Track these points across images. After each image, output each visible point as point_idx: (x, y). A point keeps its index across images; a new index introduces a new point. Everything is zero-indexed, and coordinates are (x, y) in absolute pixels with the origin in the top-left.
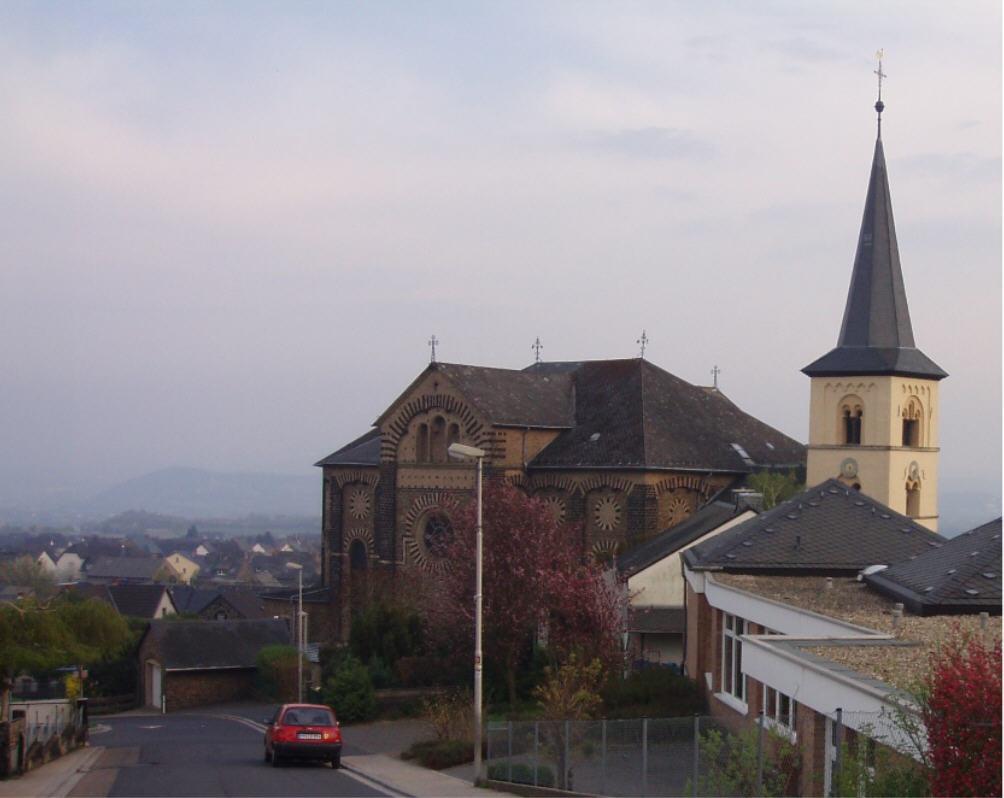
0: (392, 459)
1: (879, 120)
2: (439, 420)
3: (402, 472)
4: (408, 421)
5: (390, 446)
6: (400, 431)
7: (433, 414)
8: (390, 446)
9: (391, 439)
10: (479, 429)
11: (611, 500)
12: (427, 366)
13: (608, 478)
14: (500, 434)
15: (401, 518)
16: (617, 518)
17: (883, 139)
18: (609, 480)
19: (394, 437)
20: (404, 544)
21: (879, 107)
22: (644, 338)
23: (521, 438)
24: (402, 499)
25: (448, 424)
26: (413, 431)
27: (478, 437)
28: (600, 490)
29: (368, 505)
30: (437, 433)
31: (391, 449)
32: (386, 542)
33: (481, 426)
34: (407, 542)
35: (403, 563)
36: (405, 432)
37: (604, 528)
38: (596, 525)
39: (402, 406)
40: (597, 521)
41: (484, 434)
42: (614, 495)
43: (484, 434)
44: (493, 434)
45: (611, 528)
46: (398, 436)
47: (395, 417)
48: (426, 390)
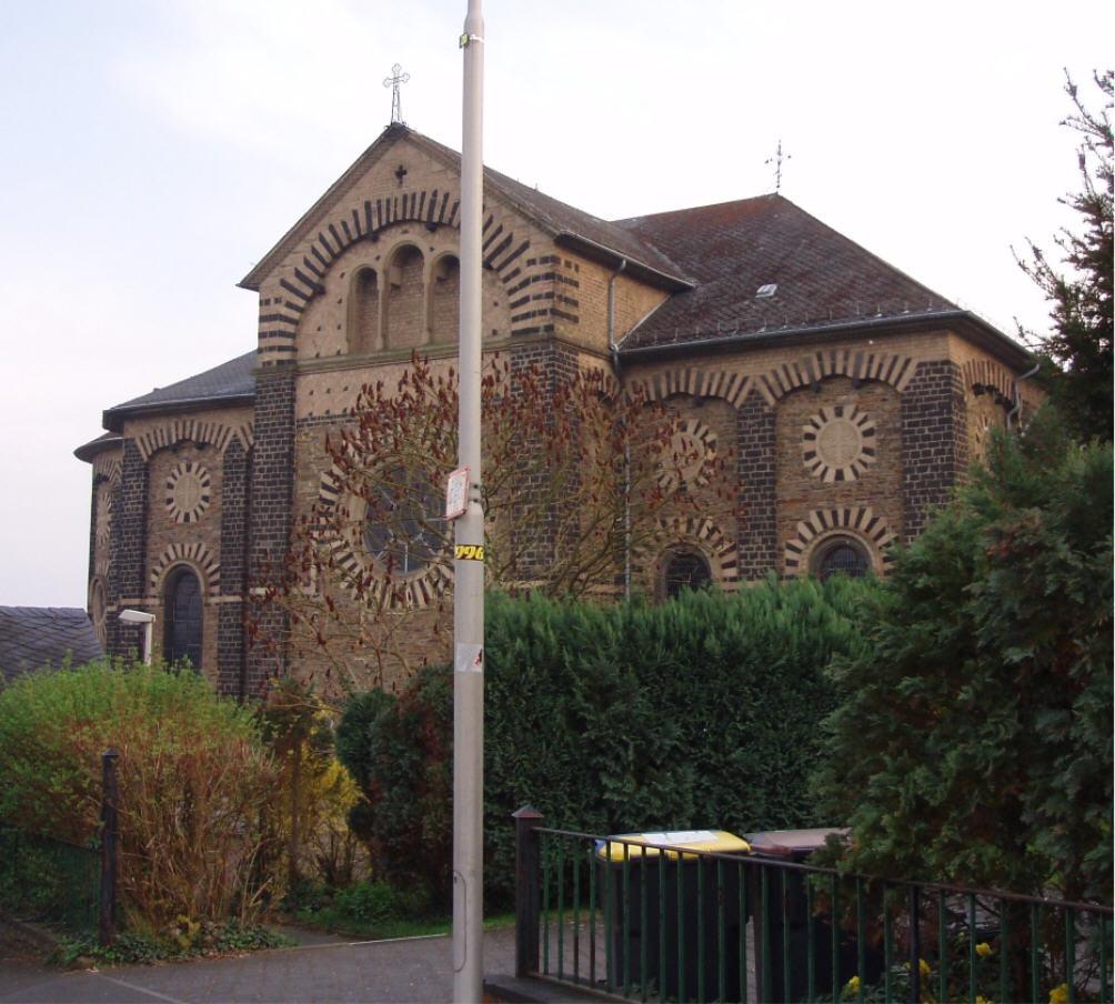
0: (286, 356)
2: (409, 255)
3: (306, 383)
4: (328, 266)
5: (282, 326)
6: (308, 291)
7: (392, 240)
8: (282, 326)
9: (284, 311)
10: (517, 254)
11: (848, 410)
13: (840, 356)
14: (568, 264)
16: (867, 451)
18: (845, 360)
19: (290, 305)
22: (779, 154)
23: (605, 285)
25: (430, 259)
26: (340, 284)
27: (516, 272)
28: (815, 388)
29: (207, 491)
30: (396, 287)
31: (282, 334)
33: (525, 246)
36: (320, 291)
37: (830, 477)
38: (805, 473)
39: (313, 235)
40: (809, 464)
41: (531, 262)
42: (854, 396)
43: (531, 262)
44: (555, 260)
45: (849, 476)
46: (301, 303)
47: (295, 261)
48: (379, 187)
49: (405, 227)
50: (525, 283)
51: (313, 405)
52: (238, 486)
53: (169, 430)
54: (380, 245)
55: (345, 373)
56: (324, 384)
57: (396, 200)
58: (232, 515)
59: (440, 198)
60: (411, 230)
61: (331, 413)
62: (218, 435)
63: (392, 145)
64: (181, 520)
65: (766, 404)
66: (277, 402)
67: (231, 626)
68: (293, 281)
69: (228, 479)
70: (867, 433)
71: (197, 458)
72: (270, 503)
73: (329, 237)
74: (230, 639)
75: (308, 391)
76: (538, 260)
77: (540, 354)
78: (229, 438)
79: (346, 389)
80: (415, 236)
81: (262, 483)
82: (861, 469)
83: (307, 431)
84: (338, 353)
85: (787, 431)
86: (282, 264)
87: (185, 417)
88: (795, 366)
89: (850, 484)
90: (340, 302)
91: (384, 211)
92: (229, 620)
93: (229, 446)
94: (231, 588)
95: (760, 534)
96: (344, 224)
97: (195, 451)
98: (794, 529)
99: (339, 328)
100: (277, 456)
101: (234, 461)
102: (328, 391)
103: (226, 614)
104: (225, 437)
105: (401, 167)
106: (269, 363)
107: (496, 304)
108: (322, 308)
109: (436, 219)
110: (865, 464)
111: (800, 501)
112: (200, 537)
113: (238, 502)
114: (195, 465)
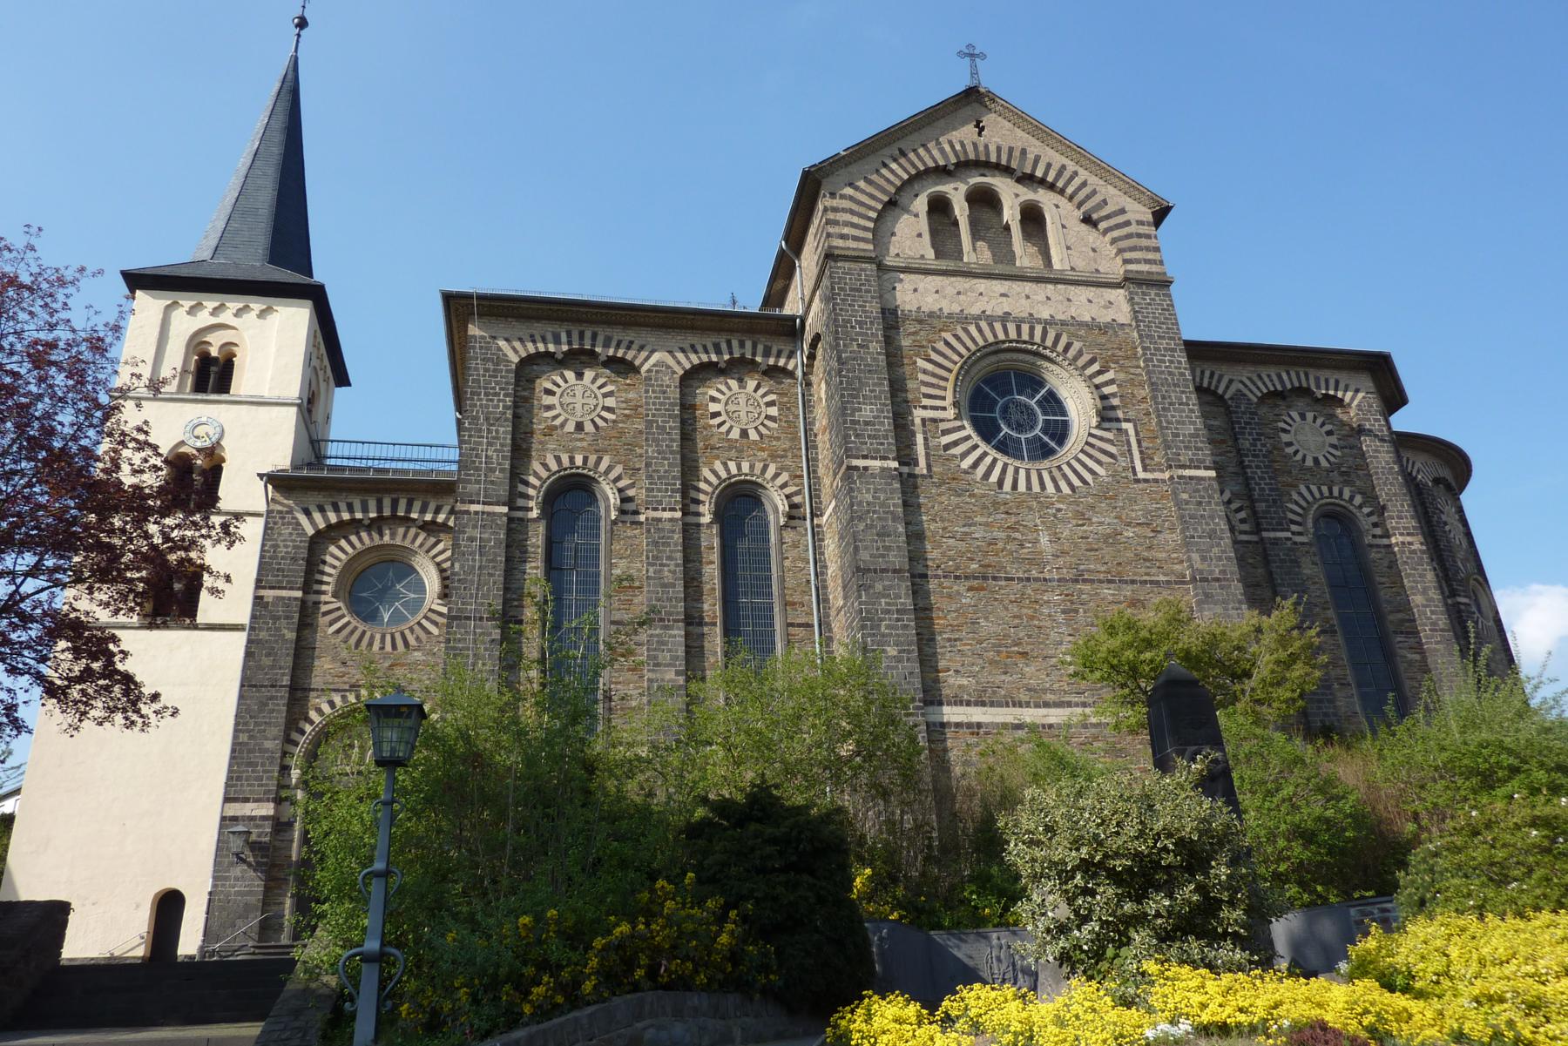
99: (920, 235)
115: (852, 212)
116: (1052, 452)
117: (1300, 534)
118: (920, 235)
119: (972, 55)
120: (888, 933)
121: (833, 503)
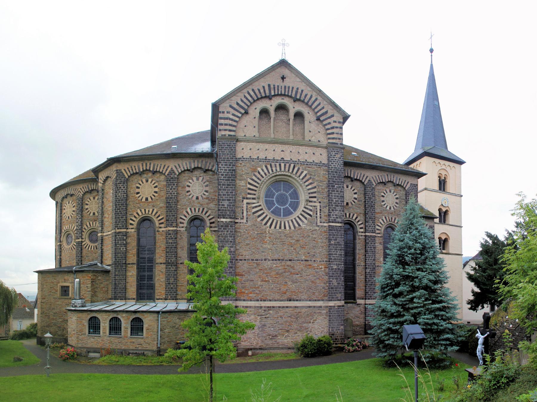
1: (432, 56)
3: (240, 146)
8: (231, 122)
10: (329, 118)
12: (278, 61)
15: (241, 183)
16: (397, 203)
17: (433, 63)
20: (245, 206)
21: (432, 51)
24: (242, 169)
26: (255, 111)
27: (329, 123)
32: (226, 203)
33: (333, 116)
34: (247, 203)
35: (245, 221)
38: (382, 206)
39: (245, 91)
40: (383, 203)
41: (335, 122)
43: (335, 122)
47: (237, 99)
48: (274, 80)
49: (283, 97)
50: (333, 128)
51: (244, 153)
52: (174, 187)
53: (139, 166)
54: (272, 101)
55: (258, 144)
56: (248, 146)
57: (281, 87)
58: (171, 198)
59: (300, 91)
60: (285, 99)
61: (252, 158)
62: (164, 168)
63: (280, 67)
64: (144, 200)
65: (373, 185)
66: (229, 150)
67: (172, 238)
68: (235, 106)
69: (169, 185)
70: (397, 198)
71: (150, 177)
72: (227, 187)
73: (252, 93)
74: (172, 243)
75: (241, 148)
76: (337, 122)
77: (339, 152)
78: (169, 169)
79: (258, 150)
80: (287, 101)
81: (223, 180)
82: (395, 207)
83: (241, 162)
84: (254, 136)
85: (376, 193)
86: (237, 95)
87: (146, 161)
88: (381, 176)
89: (392, 211)
90: (255, 118)
91: (276, 89)
92: (171, 236)
93: (169, 173)
94: (171, 225)
95: (372, 220)
96: (259, 90)
97: (150, 174)
98: (379, 220)
99: (254, 127)
100: (230, 170)
101: (172, 178)
102: (250, 149)
103: (170, 234)
104: (167, 169)
105: (283, 76)
106: (225, 135)
107: (319, 132)
108: (246, 120)
109: (298, 97)
110: (396, 206)
111: (380, 213)
112: (153, 206)
113: (174, 193)
114: (150, 180)
115: (230, 125)
116: (291, 213)
117: (379, 233)
118: (254, 127)
119: (284, 44)
120: (354, 155)
121: (173, 147)
